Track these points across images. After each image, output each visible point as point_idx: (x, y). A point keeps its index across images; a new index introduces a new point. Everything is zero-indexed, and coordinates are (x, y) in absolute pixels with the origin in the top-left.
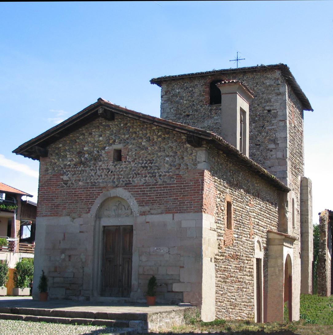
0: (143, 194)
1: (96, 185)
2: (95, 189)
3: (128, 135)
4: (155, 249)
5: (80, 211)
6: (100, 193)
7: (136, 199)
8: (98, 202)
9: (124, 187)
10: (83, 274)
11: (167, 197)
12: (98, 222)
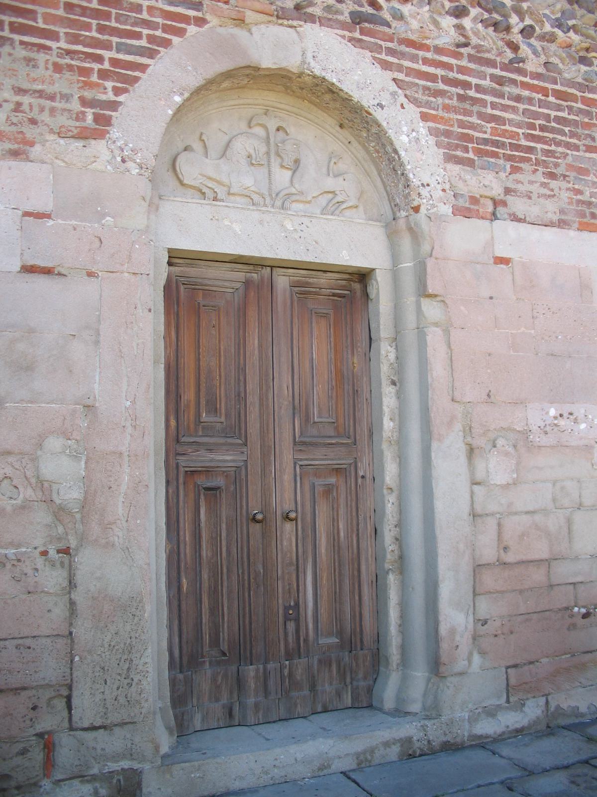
3: (416, 707)
4: (552, 412)
5: (18, 107)
6: (186, 19)
7: (424, 117)
10: (72, 603)
11: (576, 148)
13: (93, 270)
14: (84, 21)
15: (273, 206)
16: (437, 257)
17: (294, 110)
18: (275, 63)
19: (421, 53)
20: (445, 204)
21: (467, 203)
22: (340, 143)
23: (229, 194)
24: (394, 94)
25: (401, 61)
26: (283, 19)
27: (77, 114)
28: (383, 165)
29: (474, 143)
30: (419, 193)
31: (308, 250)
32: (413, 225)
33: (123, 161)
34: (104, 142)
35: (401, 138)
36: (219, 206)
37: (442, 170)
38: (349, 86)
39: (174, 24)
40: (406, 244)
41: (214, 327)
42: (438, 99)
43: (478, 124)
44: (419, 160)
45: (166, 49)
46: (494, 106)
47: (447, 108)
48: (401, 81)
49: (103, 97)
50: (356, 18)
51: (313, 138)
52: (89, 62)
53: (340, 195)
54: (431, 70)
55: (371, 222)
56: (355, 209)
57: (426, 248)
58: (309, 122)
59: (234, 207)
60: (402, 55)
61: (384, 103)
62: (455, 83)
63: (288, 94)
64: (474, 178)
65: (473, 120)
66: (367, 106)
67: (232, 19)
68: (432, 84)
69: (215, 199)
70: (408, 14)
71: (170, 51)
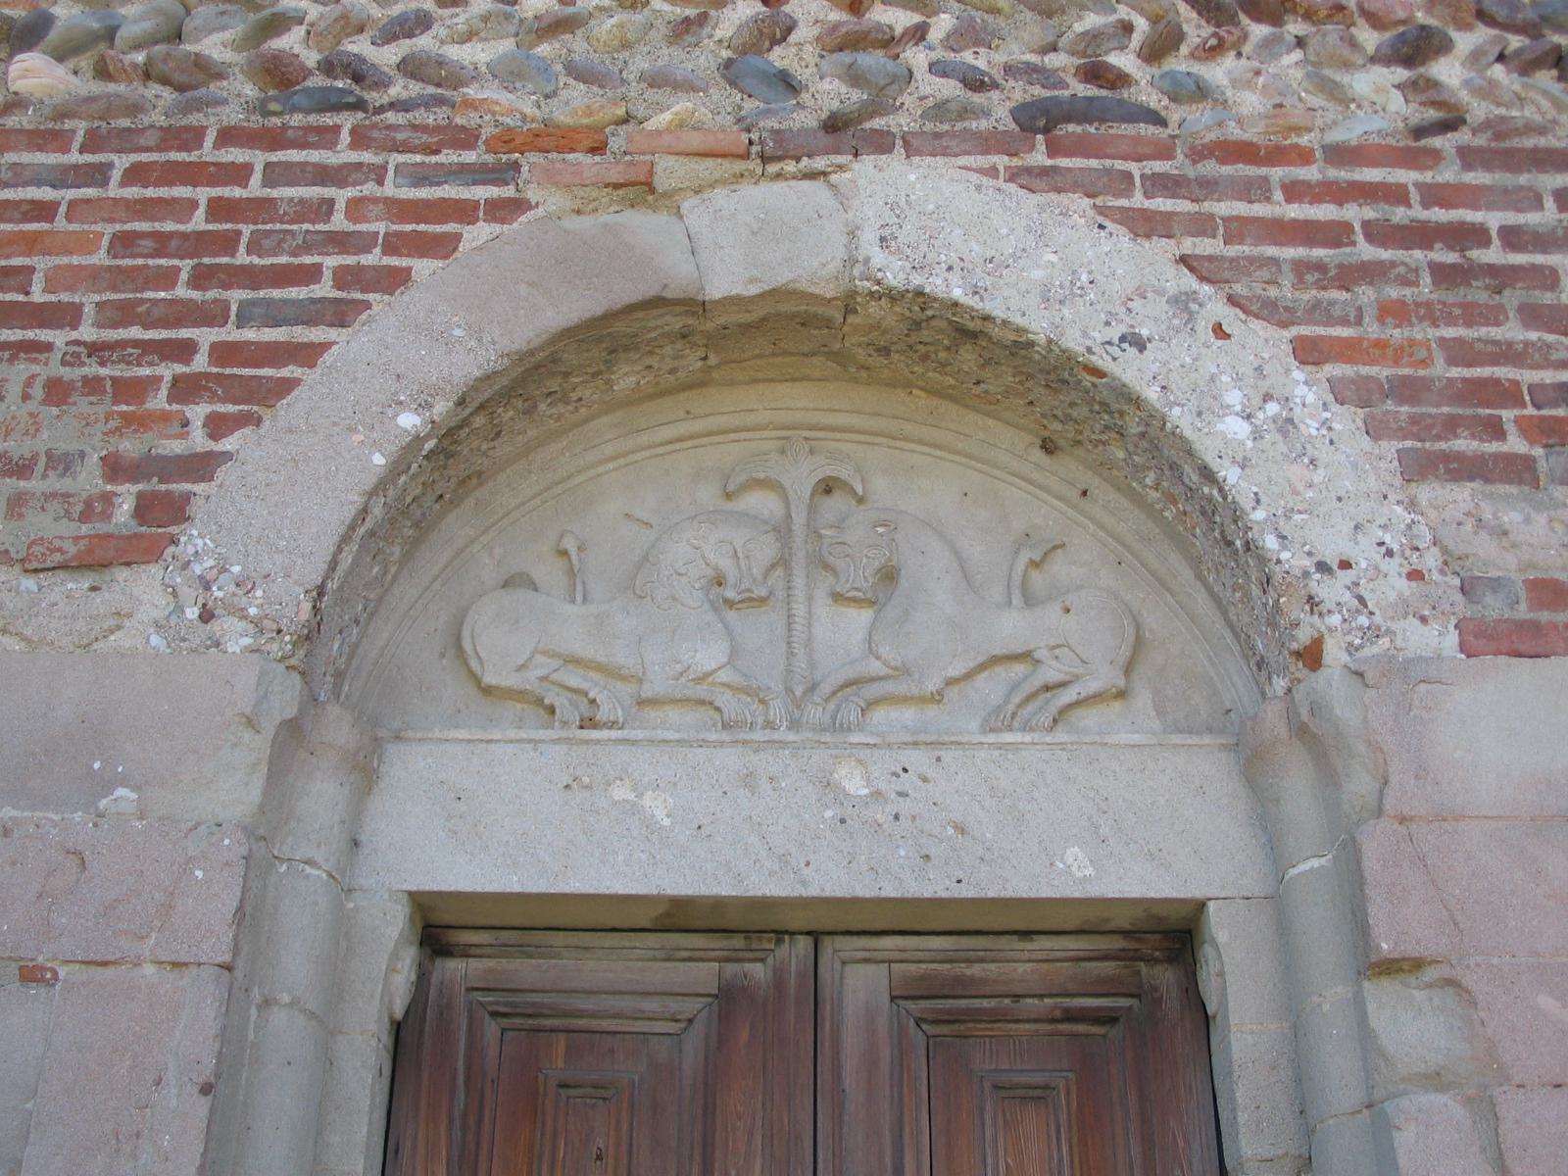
0: (1443, 275)
1: (374, 98)
2: (342, 154)
6: (465, 212)
7: (1308, 353)
8: (393, 368)
9: (989, 143)
12: (322, 795)
13: (40, 959)
14: (159, 267)
15: (794, 725)
16: (1406, 811)
17: (881, 423)
18: (753, 280)
19: (1277, 173)
20: (1424, 620)
21: (1523, 606)
22: (1055, 502)
23: (642, 703)
24: (1183, 303)
25: (1206, 204)
26: (780, 159)
27: (89, 504)
28: (1200, 544)
29: (1524, 405)
30: (1311, 598)
31: (927, 857)
32: (1305, 715)
33: (207, 616)
34: (155, 569)
35: (1220, 427)
36: (598, 742)
37: (1399, 509)
38: (1016, 302)
39: (422, 227)
40: (1297, 786)
41: (599, 1158)
42: (1359, 290)
43: (1527, 344)
44: (1301, 487)
45: (391, 294)
46: (1512, 237)
47: (1390, 312)
48: (1210, 258)
49: (176, 447)
50: (1034, 118)
51: (948, 496)
52: (151, 364)
53: (1054, 663)
54: (1325, 212)
55: (1176, 739)
56: (1117, 706)
57: (1359, 784)
58: (938, 453)
59: (651, 741)
60: (1209, 187)
61: (1145, 332)
62: (1421, 235)
63: (855, 380)
64: (1541, 519)
65: (1509, 335)
66: (1081, 349)
67: (607, 186)
68: (1331, 252)
69: (588, 723)
70: (1225, 82)
71: (403, 298)
